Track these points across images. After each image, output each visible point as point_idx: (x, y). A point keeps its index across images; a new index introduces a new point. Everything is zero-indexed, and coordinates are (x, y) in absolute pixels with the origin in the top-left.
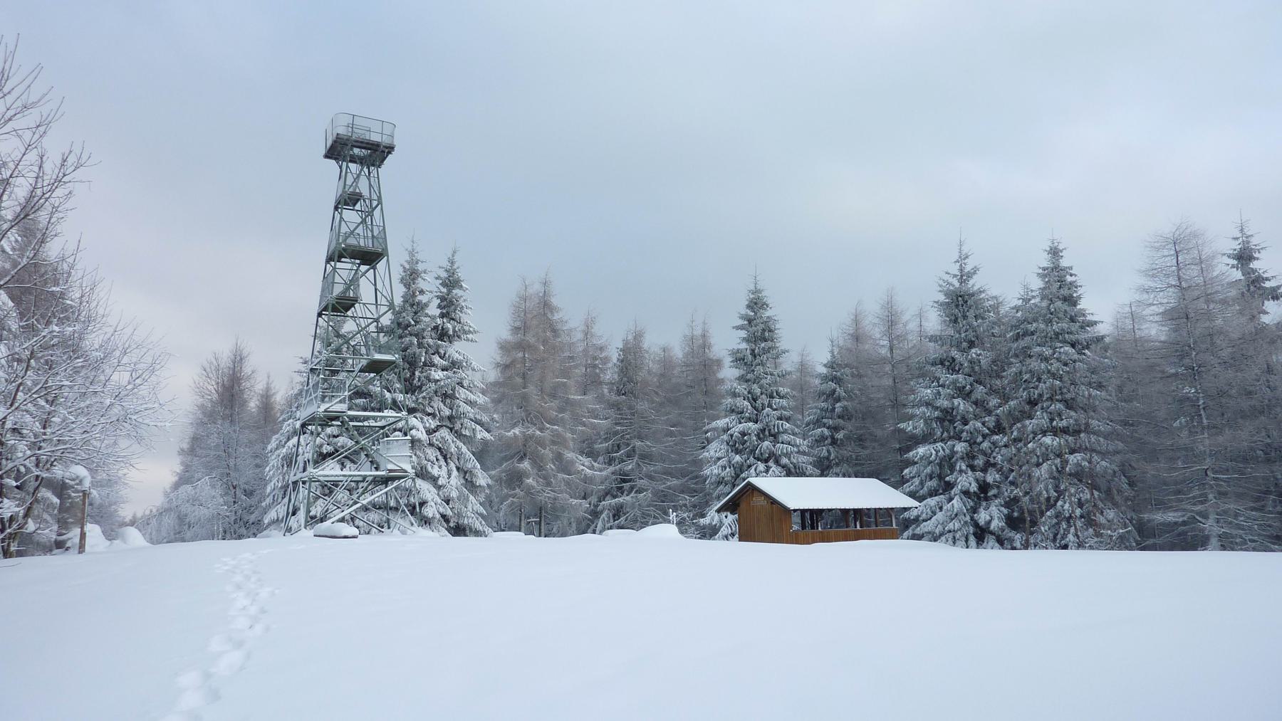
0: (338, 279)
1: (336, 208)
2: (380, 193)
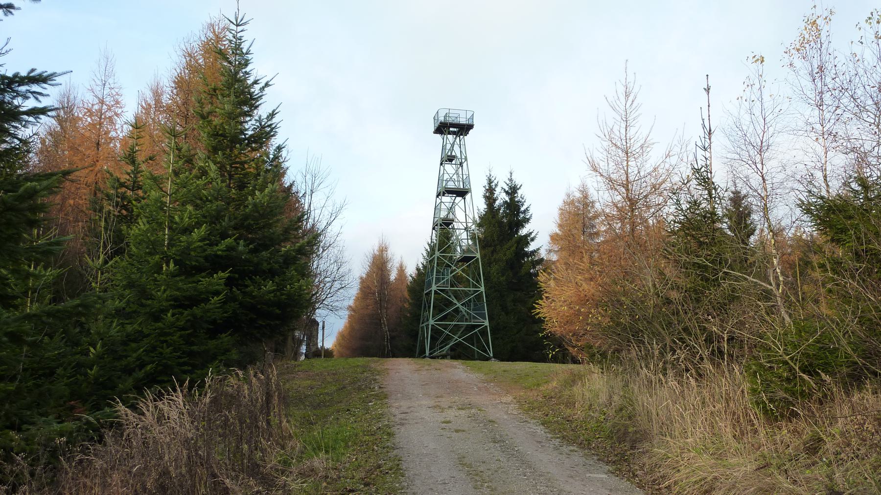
0: (443, 206)
1: (441, 164)
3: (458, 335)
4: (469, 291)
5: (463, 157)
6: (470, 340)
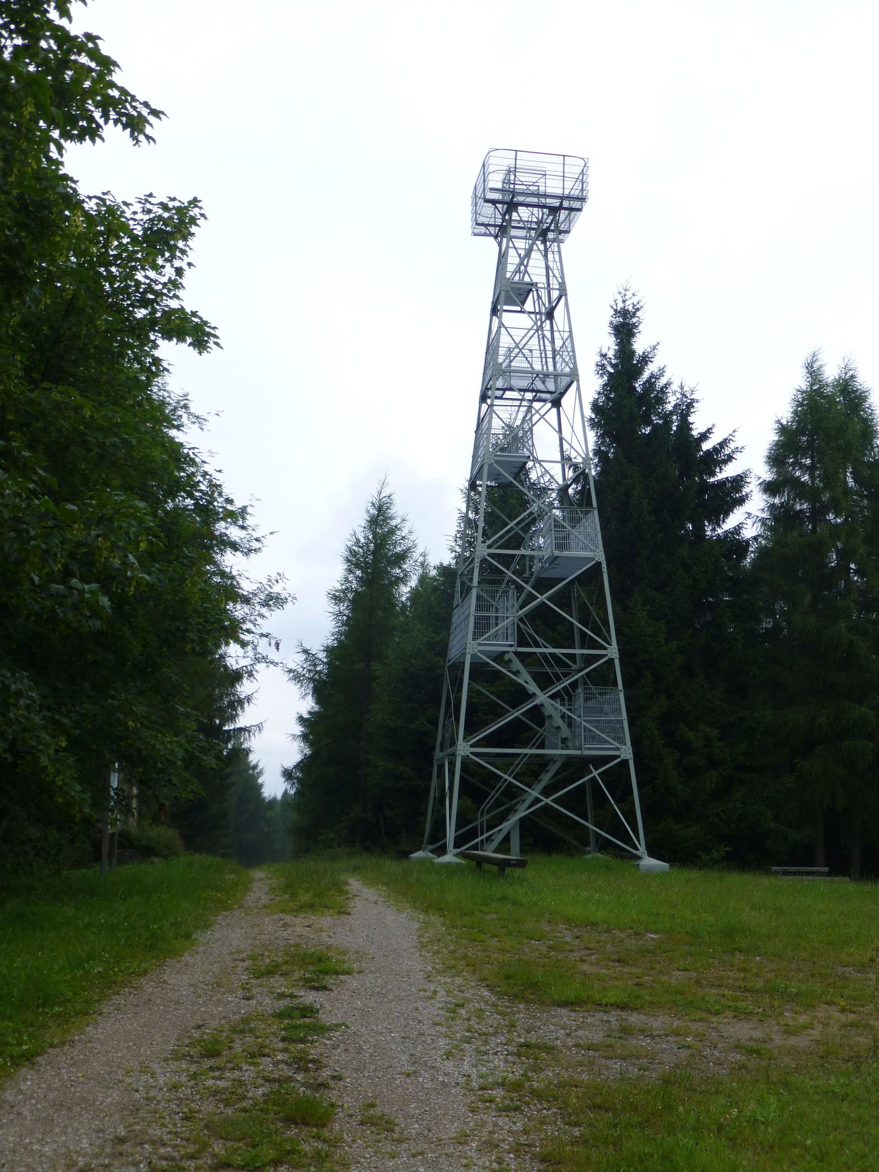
1: (494, 311)
2: (563, 277)
3: (540, 786)
4: (572, 657)
5: (554, 284)
6: (574, 801)
